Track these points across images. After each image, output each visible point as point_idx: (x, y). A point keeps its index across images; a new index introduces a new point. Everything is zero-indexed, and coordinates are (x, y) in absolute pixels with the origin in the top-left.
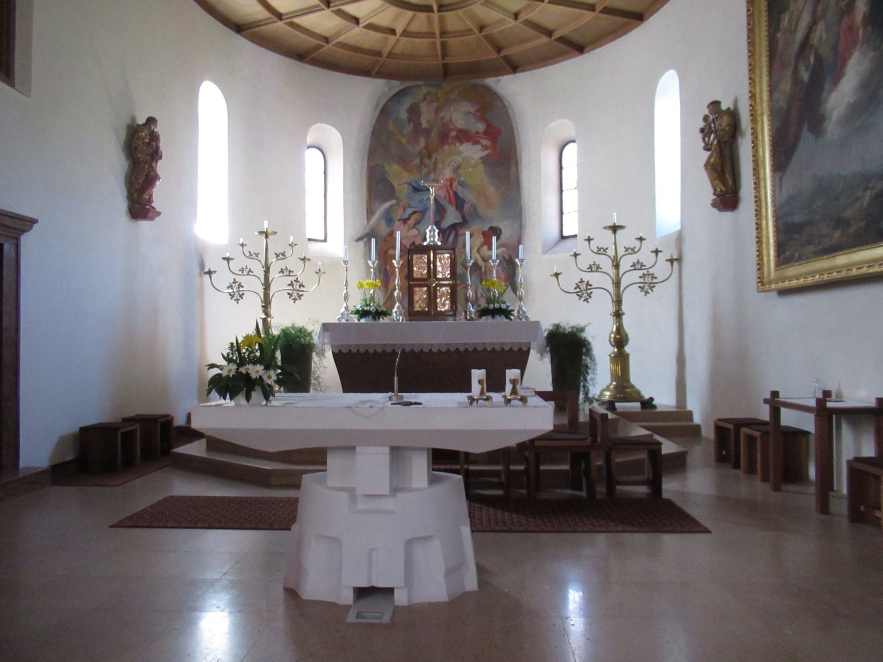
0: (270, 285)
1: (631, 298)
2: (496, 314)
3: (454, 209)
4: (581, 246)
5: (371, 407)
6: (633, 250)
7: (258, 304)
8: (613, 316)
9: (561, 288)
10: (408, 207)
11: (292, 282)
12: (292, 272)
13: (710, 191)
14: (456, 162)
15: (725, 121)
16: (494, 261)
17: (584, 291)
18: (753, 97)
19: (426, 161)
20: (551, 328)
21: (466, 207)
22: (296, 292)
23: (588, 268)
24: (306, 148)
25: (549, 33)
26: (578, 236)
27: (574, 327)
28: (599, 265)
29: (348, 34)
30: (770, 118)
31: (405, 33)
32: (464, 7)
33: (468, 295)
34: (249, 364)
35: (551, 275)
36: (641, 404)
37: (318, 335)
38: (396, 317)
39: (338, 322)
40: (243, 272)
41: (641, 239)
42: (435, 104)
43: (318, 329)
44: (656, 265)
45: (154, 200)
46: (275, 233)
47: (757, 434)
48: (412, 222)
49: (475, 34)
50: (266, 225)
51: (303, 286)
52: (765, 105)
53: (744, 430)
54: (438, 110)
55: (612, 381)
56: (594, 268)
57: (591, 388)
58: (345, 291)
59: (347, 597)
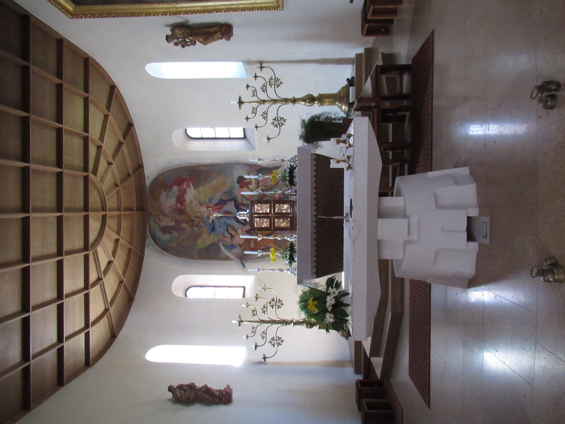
0: (273, 320)
1: (284, 92)
2: (293, 175)
3: (225, 206)
4: (250, 125)
5: (353, 229)
6: (254, 92)
7: (285, 327)
8: (295, 104)
9: (277, 136)
10: (224, 235)
11: (271, 306)
12: (264, 305)
13: (220, 41)
14: (197, 205)
15: (178, 32)
16: (260, 177)
17: (279, 122)
18: (165, 14)
19: (195, 223)
20: (302, 141)
21: (225, 198)
22: (277, 303)
23: (265, 119)
24: (186, 297)
25: (120, 144)
26: (244, 128)
27: (302, 126)
28: (263, 113)
29: (118, 268)
30: (178, 3)
31: (118, 233)
32: (104, 195)
33: (280, 193)
34: (326, 305)
35: (269, 142)
36: (350, 86)
37: (305, 287)
38: (294, 239)
39: (297, 276)
40: (264, 337)
42: (161, 217)
43: (301, 287)
44: (264, 77)
45: (219, 389)
46: (240, 316)
47: (372, 8)
48: (233, 233)
49: (119, 189)
50: (235, 322)
51: (273, 299)
52: (170, 6)
53: (369, 17)
54: (165, 215)
55: (336, 104)
56: (265, 115)
57: (340, 116)
58: (277, 271)
59: (474, 246)
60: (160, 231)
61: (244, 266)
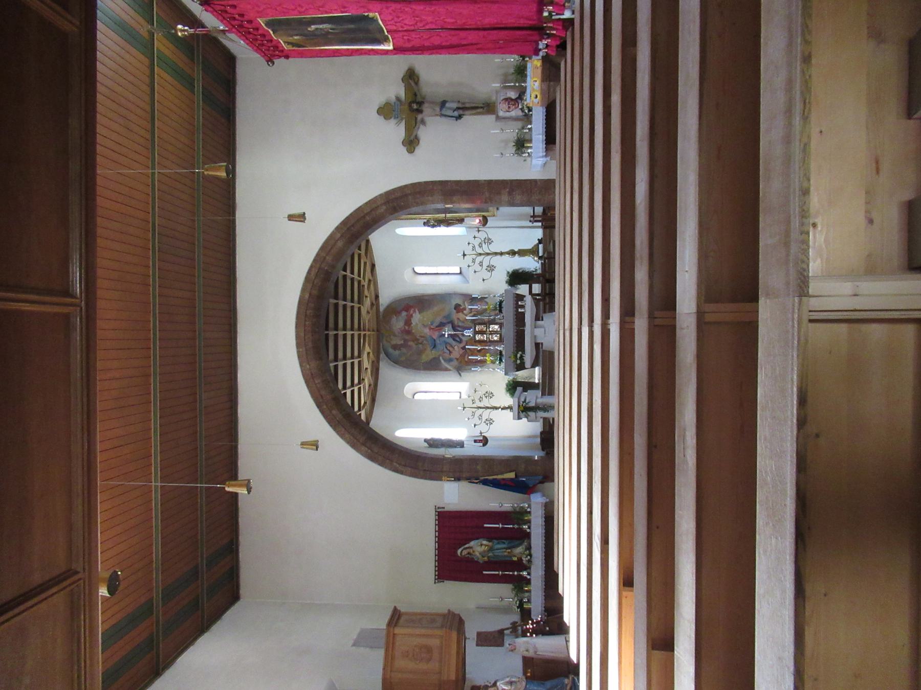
1: (494, 248)
7: (495, 411)
16: (479, 307)
17: (491, 268)
19: (420, 341)
21: (445, 321)
22: (490, 395)
41: (469, 244)
42: (392, 337)
48: (451, 349)
54: (395, 335)
56: (481, 264)
60: (392, 348)
61: (460, 375)
